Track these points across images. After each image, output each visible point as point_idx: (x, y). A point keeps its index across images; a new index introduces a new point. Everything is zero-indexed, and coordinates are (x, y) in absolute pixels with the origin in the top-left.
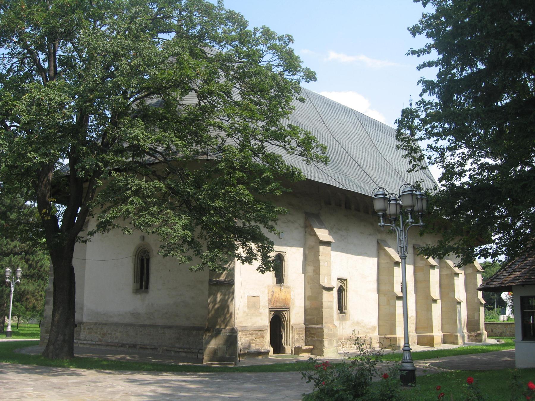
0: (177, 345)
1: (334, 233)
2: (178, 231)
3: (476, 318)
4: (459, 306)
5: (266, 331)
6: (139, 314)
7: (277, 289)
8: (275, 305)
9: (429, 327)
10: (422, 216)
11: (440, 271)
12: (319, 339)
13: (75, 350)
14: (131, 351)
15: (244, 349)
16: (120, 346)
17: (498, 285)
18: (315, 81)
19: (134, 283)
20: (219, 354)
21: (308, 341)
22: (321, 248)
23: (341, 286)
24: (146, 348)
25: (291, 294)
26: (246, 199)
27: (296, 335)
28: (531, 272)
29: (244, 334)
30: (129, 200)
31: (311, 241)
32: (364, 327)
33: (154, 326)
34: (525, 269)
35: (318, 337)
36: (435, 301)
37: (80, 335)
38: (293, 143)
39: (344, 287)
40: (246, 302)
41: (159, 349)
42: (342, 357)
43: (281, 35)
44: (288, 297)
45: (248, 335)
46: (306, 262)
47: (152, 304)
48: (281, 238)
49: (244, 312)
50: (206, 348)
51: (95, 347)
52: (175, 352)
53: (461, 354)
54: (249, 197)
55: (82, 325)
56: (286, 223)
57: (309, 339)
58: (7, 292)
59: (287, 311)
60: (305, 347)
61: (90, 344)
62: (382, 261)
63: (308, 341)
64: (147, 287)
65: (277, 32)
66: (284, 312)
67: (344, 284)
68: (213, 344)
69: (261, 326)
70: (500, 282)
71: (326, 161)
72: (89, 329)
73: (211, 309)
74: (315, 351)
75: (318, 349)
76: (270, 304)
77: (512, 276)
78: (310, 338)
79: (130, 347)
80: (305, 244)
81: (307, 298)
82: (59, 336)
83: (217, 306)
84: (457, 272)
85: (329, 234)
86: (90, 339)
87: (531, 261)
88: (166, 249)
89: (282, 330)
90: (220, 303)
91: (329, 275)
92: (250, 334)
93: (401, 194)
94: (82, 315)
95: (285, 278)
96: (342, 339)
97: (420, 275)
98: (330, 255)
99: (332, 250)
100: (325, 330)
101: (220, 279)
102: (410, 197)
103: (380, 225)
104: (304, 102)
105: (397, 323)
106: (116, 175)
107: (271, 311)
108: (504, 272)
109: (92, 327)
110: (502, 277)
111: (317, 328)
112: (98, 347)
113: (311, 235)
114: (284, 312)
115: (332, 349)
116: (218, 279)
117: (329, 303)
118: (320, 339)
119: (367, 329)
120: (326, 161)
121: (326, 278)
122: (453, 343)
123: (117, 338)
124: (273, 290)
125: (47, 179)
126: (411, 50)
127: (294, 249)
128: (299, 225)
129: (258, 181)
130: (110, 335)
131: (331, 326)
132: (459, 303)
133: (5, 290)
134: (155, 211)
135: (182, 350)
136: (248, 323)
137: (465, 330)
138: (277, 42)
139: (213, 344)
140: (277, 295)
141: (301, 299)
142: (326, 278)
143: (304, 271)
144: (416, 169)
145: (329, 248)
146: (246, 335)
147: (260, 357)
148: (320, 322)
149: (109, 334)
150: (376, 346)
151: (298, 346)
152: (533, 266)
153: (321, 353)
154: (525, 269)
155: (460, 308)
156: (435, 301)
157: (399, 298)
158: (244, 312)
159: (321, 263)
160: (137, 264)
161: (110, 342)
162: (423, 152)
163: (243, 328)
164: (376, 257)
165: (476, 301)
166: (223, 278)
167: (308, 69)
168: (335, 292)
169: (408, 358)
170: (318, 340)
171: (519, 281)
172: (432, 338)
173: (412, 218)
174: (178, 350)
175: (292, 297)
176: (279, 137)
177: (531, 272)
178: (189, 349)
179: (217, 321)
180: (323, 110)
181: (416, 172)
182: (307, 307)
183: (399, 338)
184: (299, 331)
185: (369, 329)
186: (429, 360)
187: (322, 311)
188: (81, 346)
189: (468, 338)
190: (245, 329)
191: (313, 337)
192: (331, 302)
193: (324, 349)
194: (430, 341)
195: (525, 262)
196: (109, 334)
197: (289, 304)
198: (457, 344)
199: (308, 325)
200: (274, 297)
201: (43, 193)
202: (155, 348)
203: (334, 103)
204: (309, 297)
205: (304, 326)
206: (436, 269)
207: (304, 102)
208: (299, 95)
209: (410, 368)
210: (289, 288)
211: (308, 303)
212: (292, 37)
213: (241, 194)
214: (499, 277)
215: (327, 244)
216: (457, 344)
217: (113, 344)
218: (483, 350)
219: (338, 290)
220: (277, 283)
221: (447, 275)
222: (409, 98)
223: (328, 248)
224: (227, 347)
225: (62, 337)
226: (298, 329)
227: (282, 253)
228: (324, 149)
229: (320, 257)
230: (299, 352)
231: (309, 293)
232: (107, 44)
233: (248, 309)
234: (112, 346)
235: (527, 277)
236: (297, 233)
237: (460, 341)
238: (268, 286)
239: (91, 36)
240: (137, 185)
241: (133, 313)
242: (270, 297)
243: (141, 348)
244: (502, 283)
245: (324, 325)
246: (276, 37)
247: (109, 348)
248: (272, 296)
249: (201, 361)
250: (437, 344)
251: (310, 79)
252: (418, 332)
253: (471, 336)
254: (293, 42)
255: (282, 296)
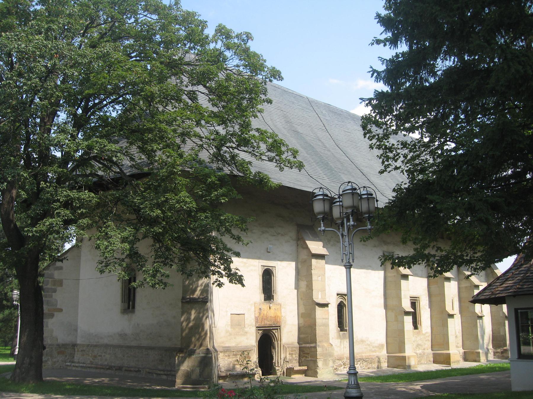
0: (160, 367)
1: (332, 245)
2: (114, 244)
3: (502, 333)
4: (481, 321)
5: (253, 351)
6: (126, 335)
7: (265, 306)
8: (263, 324)
9: (446, 345)
10: (369, 218)
11: (459, 284)
12: (312, 359)
13: (43, 376)
14: (117, 373)
15: (228, 370)
16: (108, 369)
17: (488, 297)
18: (282, 80)
19: (122, 302)
20: (194, 377)
21: (302, 362)
22: (314, 261)
23: (341, 302)
24: (131, 371)
25: (282, 311)
26: (188, 207)
27: (288, 356)
28: (525, 280)
29: (226, 354)
30: (55, 212)
31: (303, 255)
32: (369, 345)
33: (139, 347)
34: (518, 278)
35: (312, 357)
36: (452, 316)
37: (74, 357)
38: (263, 147)
39: (345, 302)
40: (229, 321)
41: (142, 371)
42: (337, 378)
43: (240, 32)
44: (279, 314)
45: (231, 356)
46: (299, 277)
47: (138, 324)
48: (269, 252)
49: (227, 332)
50: (179, 369)
51: (86, 370)
52: (157, 374)
53: (470, 374)
54: (191, 205)
55: (76, 348)
56: (274, 236)
57: (303, 359)
58: (16, 315)
59: (277, 329)
60: (297, 368)
61: (82, 367)
62: (389, 275)
63: (302, 362)
64: (134, 307)
65: (234, 30)
66: (274, 331)
67: (345, 300)
68: (186, 366)
69: (246, 347)
70: (490, 293)
71: (300, 166)
72: (82, 351)
73: (184, 327)
74: (309, 372)
75: (311, 370)
76: (257, 321)
77: (504, 285)
78: (304, 358)
79: (116, 370)
80: (297, 258)
81: (300, 315)
82: (26, 359)
83: (191, 324)
84: (477, 284)
85: (323, 247)
86: (83, 362)
87: (527, 268)
88: (103, 264)
89: (273, 350)
90: (194, 322)
91: (323, 290)
92: (234, 355)
93: (341, 193)
94: (76, 337)
95: (275, 295)
96: (343, 358)
97: (433, 287)
98: (324, 269)
99: (326, 263)
100: (319, 350)
101: (194, 296)
102: (351, 196)
103: (320, 230)
104: (271, 103)
105: (406, 340)
106: (45, 185)
107: (258, 330)
108: (497, 282)
109: (84, 349)
110: (494, 287)
111: (311, 347)
112: (88, 370)
113: (303, 248)
114: (274, 331)
115: (327, 370)
116: (191, 297)
117: (324, 321)
118: (314, 359)
119: (373, 347)
120: (300, 166)
121: (320, 293)
122: (475, 361)
123: (106, 360)
124: (260, 307)
125: (11, 195)
126: (375, 39)
127: (285, 264)
128: (291, 237)
129: (203, 187)
130: (100, 358)
131: (326, 345)
132: (481, 317)
133: (14, 313)
134: (85, 224)
135: (162, 373)
136: (232, 343)
137: (490, 347)
138: (236, 41)
139: (186, 366)
140: (265, 313)
141: (294, 316)
142: (320, 293)
143: (297, 287)
144: (388, 170)
145: (324, 261)
146: (229, 356)
147: (246, 380)
148: (314, 341)
149: (99, 356)
150: (384, 365)
151: (291, 366)
152: (527, 273)
153: (315, 374)
154: (518, 278)
155: (482, 322)
156: (452, 316)
157: (407, 313)
158: (227, 332)
159: (314, 278)
160: (125, 283)
161: (101, 365)
162: (398, 151)
163: (225, 349)
164: (381, 270)
165: (501, 315)
166: (197, 294)
167: (274, 68)
168: (333, 310)
169: (353, 383)
170: (311, 360)
171: (511, 291)
172: (448, 356)
173: (353, 221)
174: (159, 372)
175: (283, 314)
176: (244, 142)
177: (525, 280)
178: (171, 371)
179: (191, 341)
180: (328, 118)
181: (389, 172)
182: (301, 325)
183: (408, 356)
184: (292, 351)
185: (376, 347)
186: (427, 381)
187: (315, 329)
188: (74, 368)
189: (494, 355)
190: (227, 350)
191: (306, 357)
192: (326, 319)
193: (318, 370)
194: (447, 359)
195: (521, 269)
196: (99, 356)
197: (280, 322)
198: (479, 361)
199: (302, 344)
200: (262, 315)
201: (6, 210)
202: (139, 371)
203: (342, 111)
204: (302, 314)
205: (298, 345)
206: (451, 282)
207: (271, 103)
208: (265, 96)
209: (357, 395)
210: (280, 305)
211: (302, 321)
212: (250, 34)
213: (181, 202)
214: (491, 288)
215: (321, 257)
216: (479, 361)
217: (101, 367)
218: (503, 368)
219: (338, 306)
220: (265, 300)
221: (466, 287)
223: (322, 262)
224: (200, 370)
225: (28, 361)
226: (290, 349)
227: (271, 268)
228: (295, 153)
229: (313, 272)
230: (291, 373)
231: (302, 310)
232: (21, 45)
233: (231, 328)
234: (100, 368)
235: (520, 286)
236: (289, 247)
237: (483, 359)
238: (255, 303)
239: (12, 38)
240: (65, 196)
241: (121, 334)
242: (257, 315)
243: (126, 370)
244: (493, 293)
245: (318, 343)
246: (233, 35)
247: (98, 371)
248: (260, 313)
249: (174, 383)
250: (454, 362)
251: (275, 78)
252: (434, 349)
253: (497, 352)
254: (252, 40)
255: (272, 313)
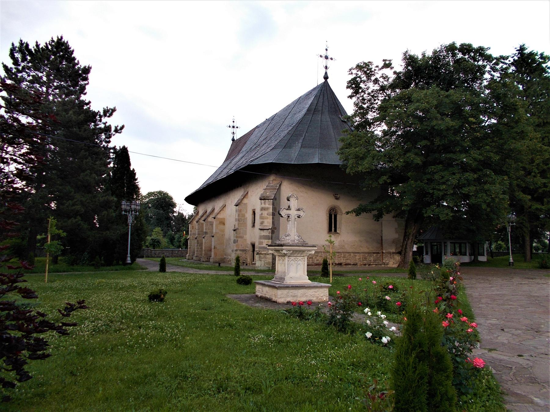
130: (311, 259)
222: (233, 118)
